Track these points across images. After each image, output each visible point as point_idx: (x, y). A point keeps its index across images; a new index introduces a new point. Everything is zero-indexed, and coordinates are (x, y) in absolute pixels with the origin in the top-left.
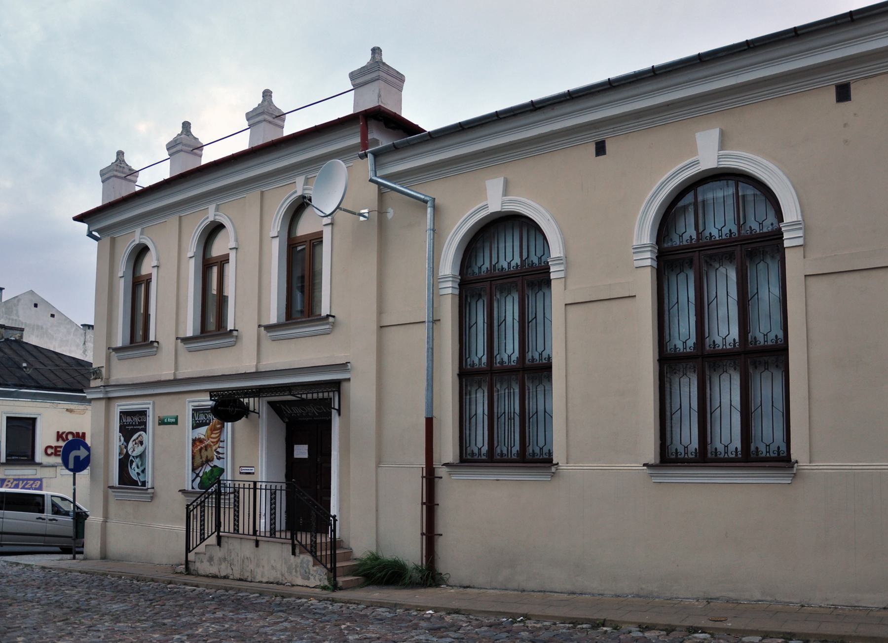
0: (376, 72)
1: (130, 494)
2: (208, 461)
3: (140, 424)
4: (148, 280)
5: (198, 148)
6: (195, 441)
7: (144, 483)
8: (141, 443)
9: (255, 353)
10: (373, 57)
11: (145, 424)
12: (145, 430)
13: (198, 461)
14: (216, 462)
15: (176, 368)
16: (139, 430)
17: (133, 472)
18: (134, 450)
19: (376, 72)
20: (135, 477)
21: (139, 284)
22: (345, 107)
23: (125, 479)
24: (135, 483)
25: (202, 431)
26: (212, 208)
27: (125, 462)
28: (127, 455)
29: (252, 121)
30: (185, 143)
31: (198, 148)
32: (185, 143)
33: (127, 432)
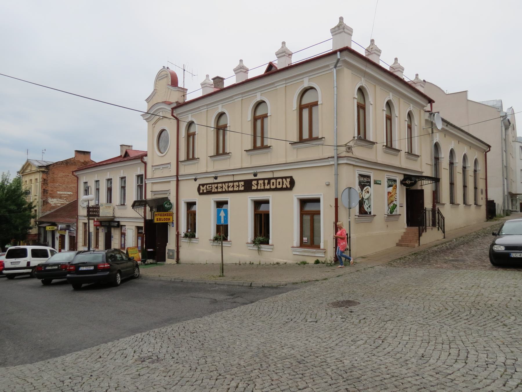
0: (341, 29)
1: (364, 218)
2: (392, 201)
3: (367, 182)
4: (194, 134)
5: (247, 71)
6: (389, 193)
7: (370, 213)
8: (368, 192)
9: (240, 159)
10: (340, 22)
11: (370, 182)
12: (370, 186)
13: (389, 201)
14: (395, 202)
15: (242, 164)
16: (366, 185)
17: (366, 207)
18: (366, 196)
19: (341, 29)
20: (366, 210)
21: (190, 136)
22: (328, 48)
23: (362, 212)
24: (366, 213)
25: (391, 188)
26: (220, 106)
27: (361, 203)
28: (363, 198)
29: (278, 56)
30: (241, 69)
31: (247, 71)
32: (241, 69)
33: (362, 186)
